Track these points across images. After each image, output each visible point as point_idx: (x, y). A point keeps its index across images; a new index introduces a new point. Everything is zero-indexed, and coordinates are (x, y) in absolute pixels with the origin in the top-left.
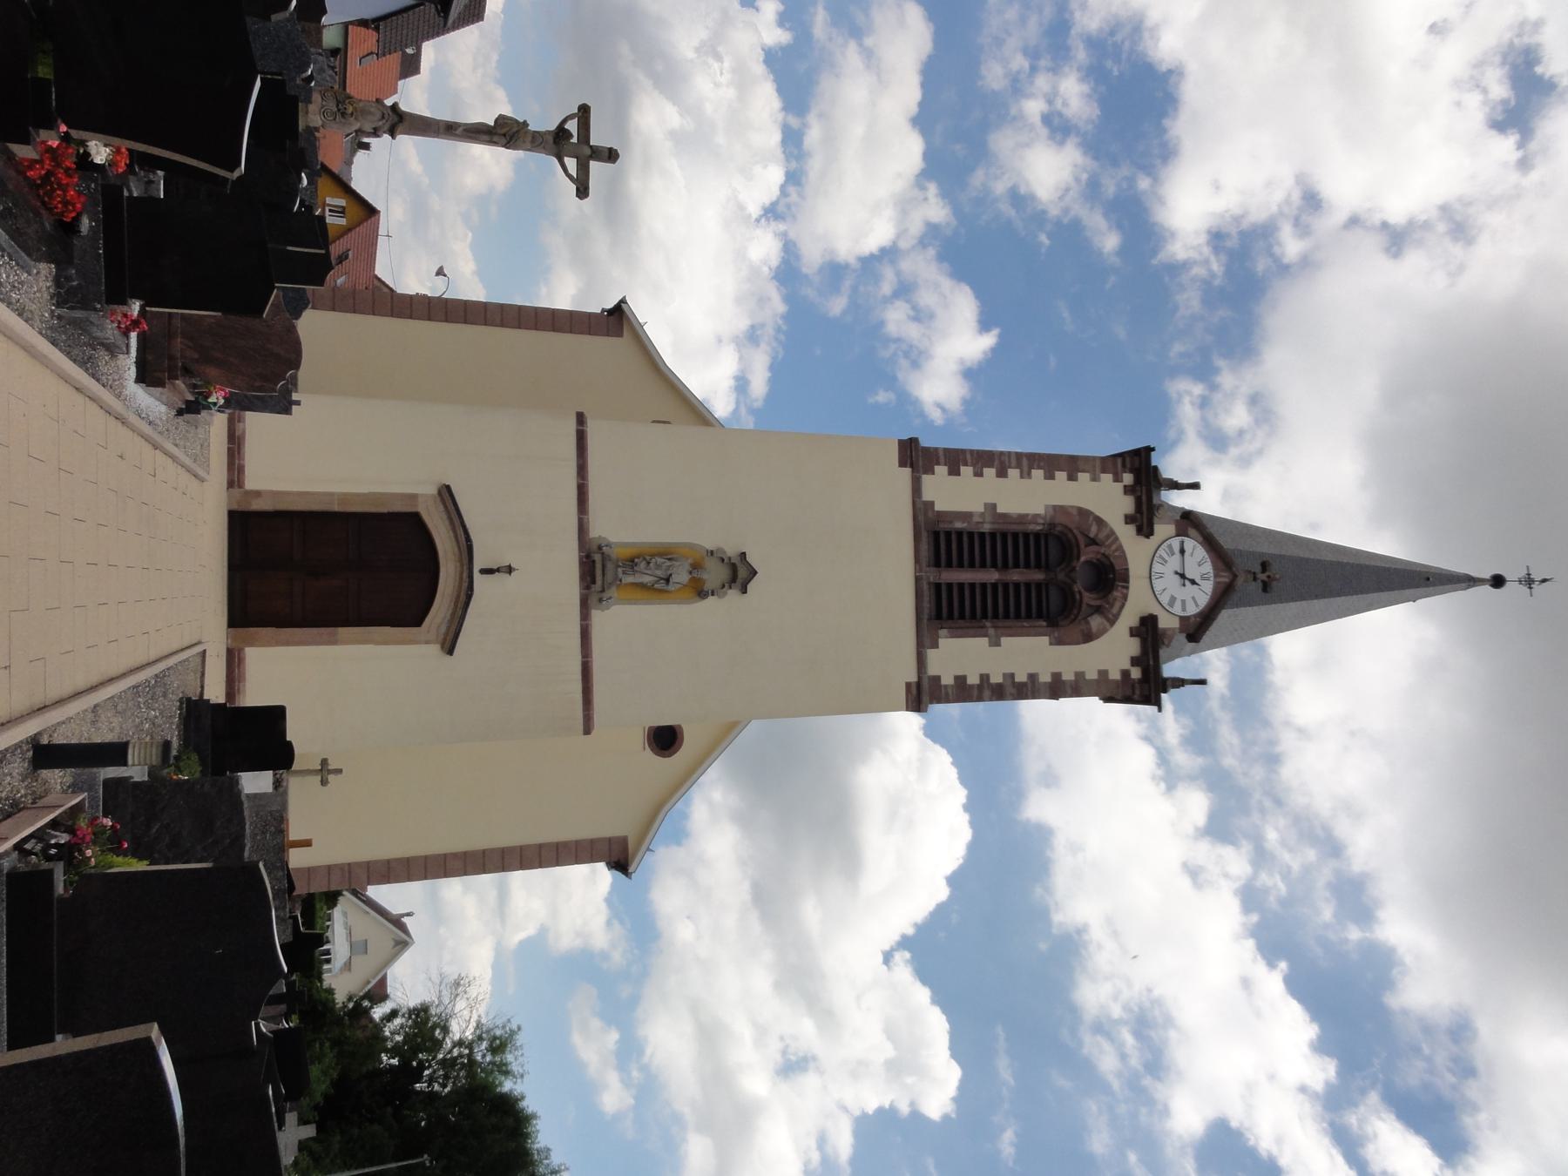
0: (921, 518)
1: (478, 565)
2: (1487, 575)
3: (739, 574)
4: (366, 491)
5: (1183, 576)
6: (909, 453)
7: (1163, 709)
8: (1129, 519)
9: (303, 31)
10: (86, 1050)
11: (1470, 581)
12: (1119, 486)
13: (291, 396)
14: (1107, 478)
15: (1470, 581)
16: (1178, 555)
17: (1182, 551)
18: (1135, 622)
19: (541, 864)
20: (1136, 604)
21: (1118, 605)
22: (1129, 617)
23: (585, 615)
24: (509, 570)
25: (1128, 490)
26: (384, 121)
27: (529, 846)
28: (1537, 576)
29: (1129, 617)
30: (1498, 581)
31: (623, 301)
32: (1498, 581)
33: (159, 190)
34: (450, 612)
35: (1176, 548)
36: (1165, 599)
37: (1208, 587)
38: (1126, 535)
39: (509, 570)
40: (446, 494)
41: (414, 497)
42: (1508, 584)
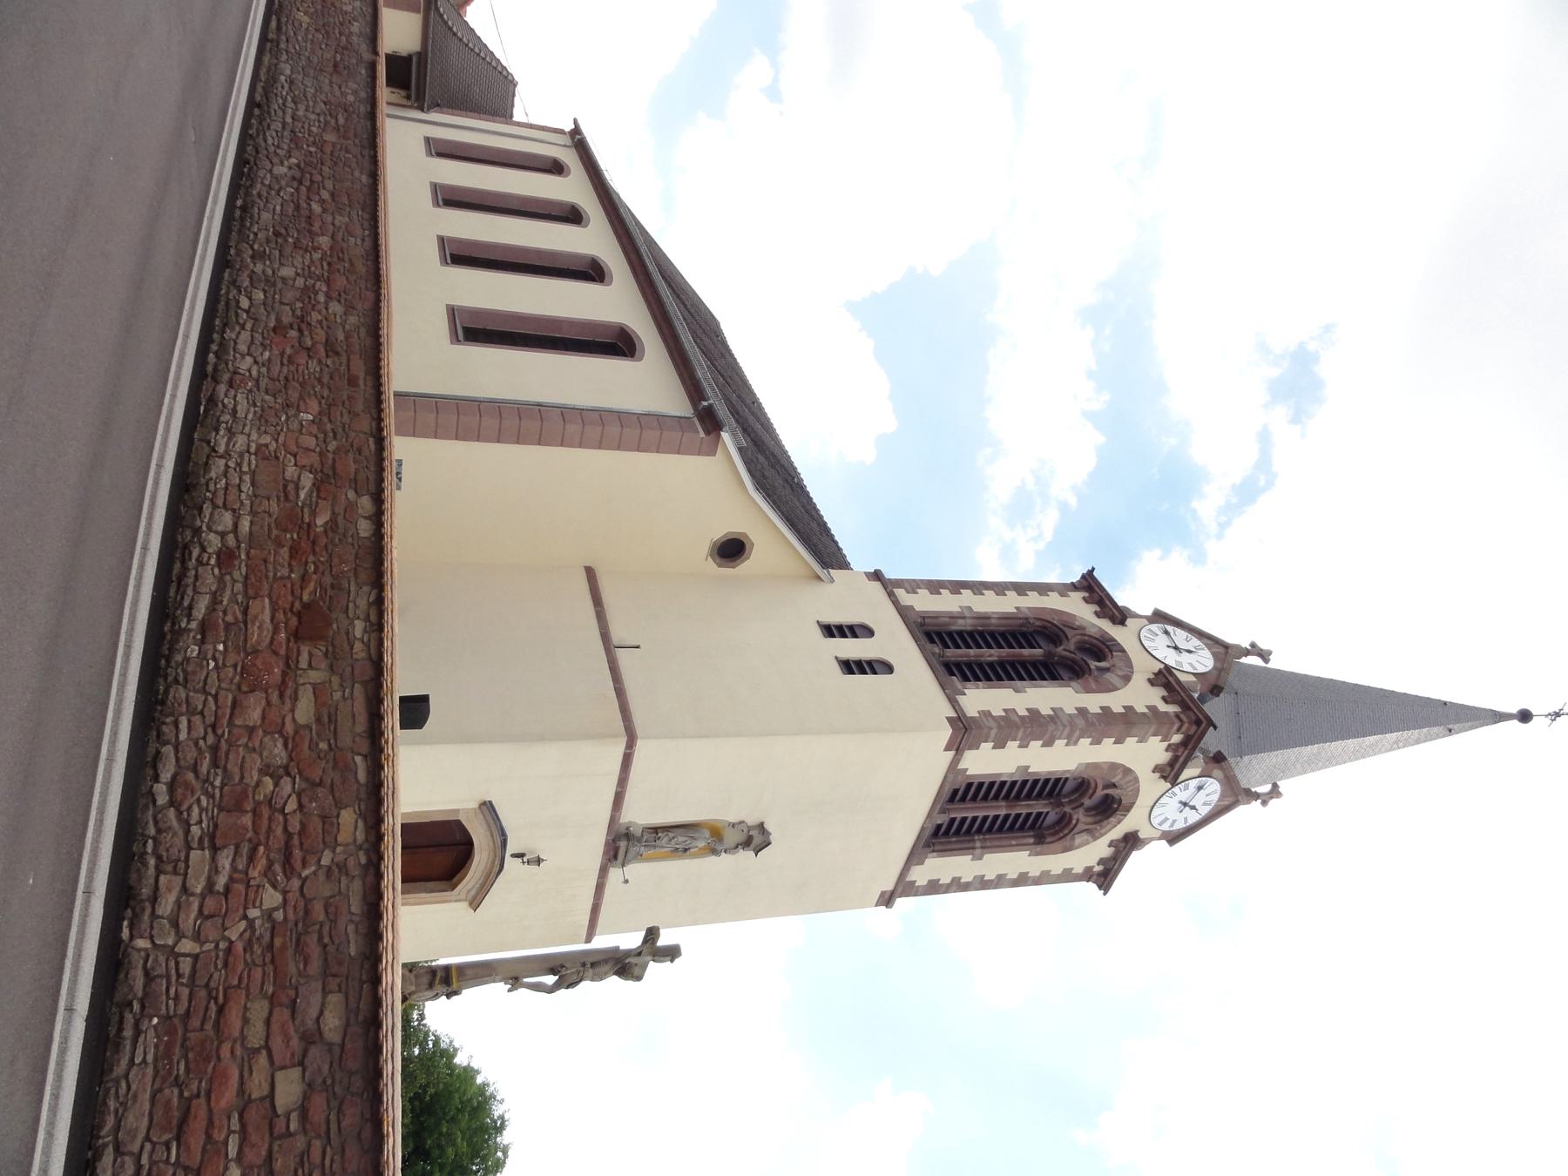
0: (951, 777)
1: (510, 850)
2: (1514, 710)
4: (410, 811)
5: (1176, 648)
6: (959, 740)
7: (1218, 725)
11: (1498, 717)
15: (1498, 717)
21: (1109, 827)
23: (603, 872)
24: (755, 839)
26: (268, 348)
30: (1525, 716)
31: (945, 750)
32: (1525, 716)
34: (480, 882)
39: (755, 839)
40: (488, 808)
41: (456, 811)
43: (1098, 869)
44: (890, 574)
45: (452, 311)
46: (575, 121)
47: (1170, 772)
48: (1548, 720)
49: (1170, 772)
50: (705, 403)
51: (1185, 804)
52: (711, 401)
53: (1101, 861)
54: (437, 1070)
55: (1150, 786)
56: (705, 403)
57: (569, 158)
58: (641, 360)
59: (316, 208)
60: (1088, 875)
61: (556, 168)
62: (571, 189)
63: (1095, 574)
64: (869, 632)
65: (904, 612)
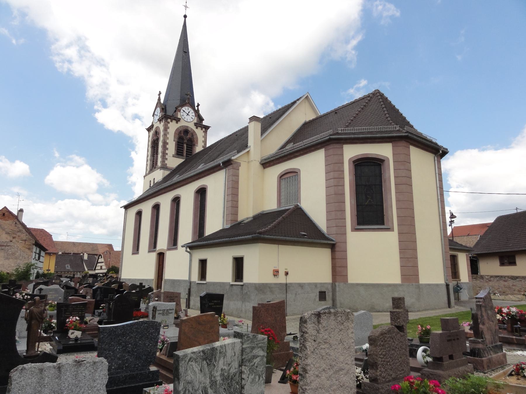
2: (184, 18)
3: (154, 179)
8: (177, 123)
9: (402, 314)
10: (182, 77)
12: (170, 123)
13: (57, 321)
14: (169, 125)
16: (184, 112)
17: (184, 111)
18: (195, 127)
19: (415, 257)
20: (192, 126)
22: (194, 128)
25: (171, 121)
27: (399, 239)
28: (185, 4)
29: (194, 128)
30: (185, 16)
32: (185, 16)
33: (172, 305)
35: (183, 112)
36: (192, 120)
37: (190, 109)
38: (180, 124)
42: (186, 14)
43: (204, 130)
44: (144, 174)
45: (133, 254)
46: (121, 207)
47: (178, 120)
48: (187, 9)
49: (178, 120)
50: (221, 164)
51: (188, 114)
52: (221, 162)
53: (202, 129)
54: (400, 304)
55: (180, 124)
56: (221, 164)
57: (133, 211)
58: (160, 203)
59: (19, 252)
60: (206, 132)
61: (139, 214)
62: (147, 208)
63: (147, 128)
64: (150, 181)
65: (149, 173)
